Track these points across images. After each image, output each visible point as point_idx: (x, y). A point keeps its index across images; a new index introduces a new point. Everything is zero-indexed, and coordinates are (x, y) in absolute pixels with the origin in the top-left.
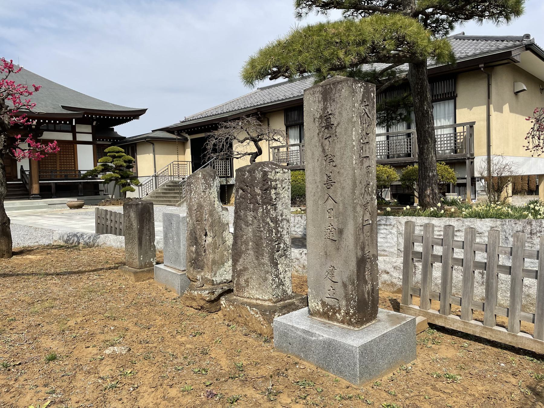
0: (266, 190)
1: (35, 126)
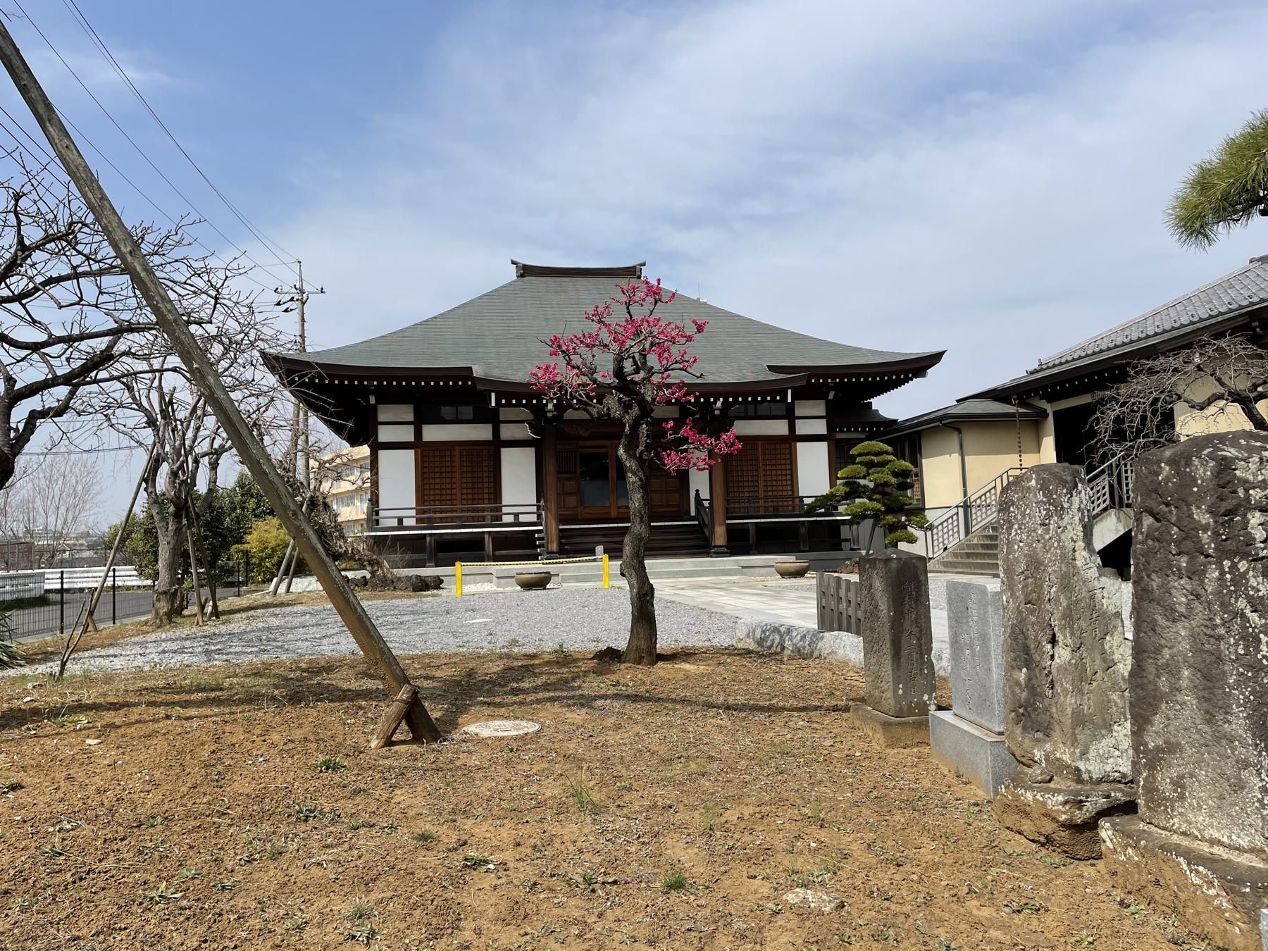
0: (1230, 512)
1: (711, 408)
